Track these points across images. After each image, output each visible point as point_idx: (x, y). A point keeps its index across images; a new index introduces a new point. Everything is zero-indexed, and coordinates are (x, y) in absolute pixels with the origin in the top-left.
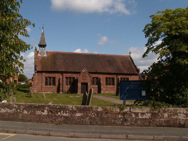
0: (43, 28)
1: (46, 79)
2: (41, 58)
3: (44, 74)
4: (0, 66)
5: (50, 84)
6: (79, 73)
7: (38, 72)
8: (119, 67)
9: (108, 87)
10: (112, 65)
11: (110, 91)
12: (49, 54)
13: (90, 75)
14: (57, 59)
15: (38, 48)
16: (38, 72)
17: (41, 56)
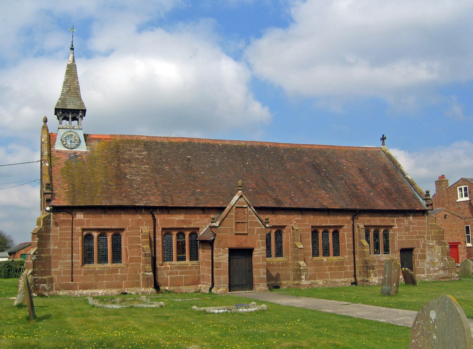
0: (72, 49)
1: (88, 238)
2: (65, 158)
3: (79, 216)
4: (472, 240)
5: (103, 259)
6: (222, 209)
7: (57, 209)
8: (354, 185)
9: (320, 263)
10: (328, 181)
11: (332, 276)
12: (95, 144)
13: (264, 217)
14: (129, 161)
15: (53, 120)
16: (57, 209)
17: (66, 152)
